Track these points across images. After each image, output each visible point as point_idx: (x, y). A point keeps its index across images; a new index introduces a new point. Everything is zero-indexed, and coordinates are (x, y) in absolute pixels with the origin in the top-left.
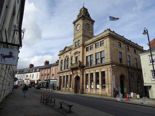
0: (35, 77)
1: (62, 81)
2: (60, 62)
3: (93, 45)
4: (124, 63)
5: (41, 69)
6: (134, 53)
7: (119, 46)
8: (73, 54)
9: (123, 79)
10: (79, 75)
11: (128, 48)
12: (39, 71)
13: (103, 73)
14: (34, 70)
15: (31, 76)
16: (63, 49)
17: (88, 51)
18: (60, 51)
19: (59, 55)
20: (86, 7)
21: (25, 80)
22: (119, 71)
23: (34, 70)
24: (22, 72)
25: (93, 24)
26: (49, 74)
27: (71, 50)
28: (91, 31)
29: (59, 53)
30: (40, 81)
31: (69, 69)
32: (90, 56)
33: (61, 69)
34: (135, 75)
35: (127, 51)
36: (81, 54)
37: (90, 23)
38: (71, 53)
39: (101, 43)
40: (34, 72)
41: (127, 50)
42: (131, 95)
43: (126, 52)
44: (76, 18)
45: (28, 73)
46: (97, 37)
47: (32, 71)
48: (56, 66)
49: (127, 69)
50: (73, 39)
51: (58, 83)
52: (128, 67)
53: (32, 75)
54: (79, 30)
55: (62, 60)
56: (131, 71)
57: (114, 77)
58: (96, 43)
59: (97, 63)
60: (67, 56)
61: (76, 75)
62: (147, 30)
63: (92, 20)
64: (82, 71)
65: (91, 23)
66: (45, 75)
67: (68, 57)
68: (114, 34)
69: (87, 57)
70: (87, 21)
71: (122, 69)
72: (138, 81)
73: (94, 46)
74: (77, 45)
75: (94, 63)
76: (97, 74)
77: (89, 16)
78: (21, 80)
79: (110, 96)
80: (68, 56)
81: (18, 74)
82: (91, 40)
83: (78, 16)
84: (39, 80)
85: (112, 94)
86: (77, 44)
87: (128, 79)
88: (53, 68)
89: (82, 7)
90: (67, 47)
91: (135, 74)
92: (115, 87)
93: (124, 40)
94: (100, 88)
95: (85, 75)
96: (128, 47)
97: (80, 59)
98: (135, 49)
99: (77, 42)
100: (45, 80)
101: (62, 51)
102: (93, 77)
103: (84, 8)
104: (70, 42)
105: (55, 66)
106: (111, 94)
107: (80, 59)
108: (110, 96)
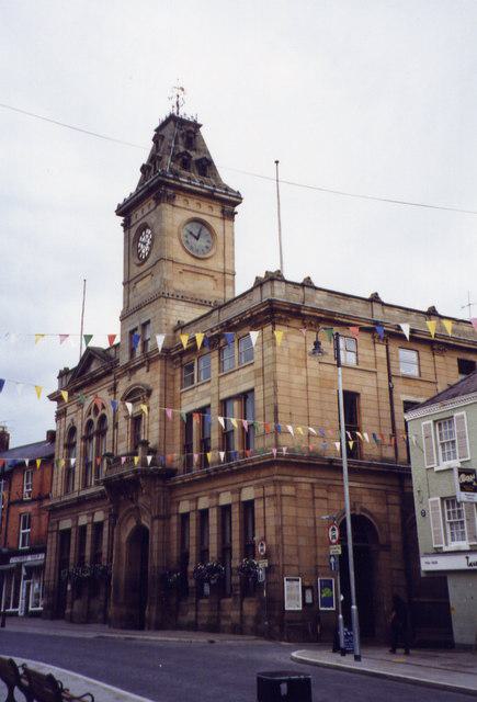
13: (248, 506)
20: (187, 112)
25: (229, 215)
50: (119, 307)
54: (146, 258)
55: (72, 431)
61: (132, 524)
65: (219, 214)
70: (193, 204)
77: (206, 166)
80: (104, 407)
107: (152, 434)
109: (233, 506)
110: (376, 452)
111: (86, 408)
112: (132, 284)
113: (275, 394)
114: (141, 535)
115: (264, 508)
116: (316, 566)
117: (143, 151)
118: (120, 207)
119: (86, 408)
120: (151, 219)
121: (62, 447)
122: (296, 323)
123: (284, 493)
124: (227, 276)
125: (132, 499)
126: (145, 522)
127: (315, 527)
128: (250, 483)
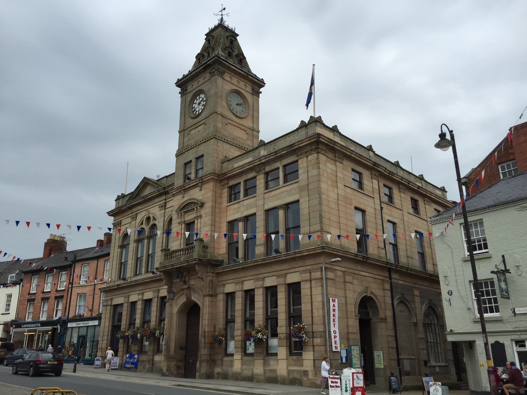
1: (124, 313)
3: (255, 177)
4: (373, 249)
6: (411, 211)
7: (355, 185)
8: (177, 211)
9: (371, 316)
16: (131, 188)
17: (235, 200)
20: (229, 23)
22: (356, 282)
26: (62, 297)
27: (166, 193)
28: (248, 123)
29: (112, 206)
31: (153, 273)
32: (246, 219)
34: (417, 299)
35: (383, 205)
37: (246, 88)
38: (164, 207)
39: (289, 169)
41: (385, 199)
42: (110, 350)
43: (382, 208)
46: (271, 149)
48: (97, 258)
49: (387, 275)
50: (175, 147)
51: (106, 333)
52: (390, 269)
54: (200, 114)
56: (400, 282)
57: (336, 308)
58: (268, 169)
59: (271, 247)
60: (148, 219)
61: (182, 300)
62: (451, 132)
63: (255, 77)
65: (250, 91)
66: (45, 299)
67: (151, 223)
68: (337, 139)
69: (232, 224)
70: (235, 80)
71: (365, 273)
72: (427, 322)
73: (260, 181)
74: (193, 176)
76: (271, 292)
77: (241, 59)
80: (155, 219)
82: (250, 159)
84: (17, 323)
86: (193, 171)
87: (389, 313)
88: (84, 273)
90: (148, 179)
91: (417, 293)
92: (338, 345)
93: (375, 164)
94: (282, 352)
96: (390, 189)
98: (416, 197)
100: (43, 324)
102: (275, 305)
103: (221, 26)
107: (203, 228)
109: (301, 283)
110: (376, 252)
111: (139, 220)
112: (186, 132)
113: (320, 203)
114: (192, 311)
115: (311, 288)
116: (348, 333)
117: (199, 43)
118: (179, 80)
119: (139, 220)
120: (204, 87)
121: (117, 247)
123: (328, 277)
124: (255, 131)
125: (185, 282)
126: (195, 298)
127: (346, 304)
128: (297, 269)
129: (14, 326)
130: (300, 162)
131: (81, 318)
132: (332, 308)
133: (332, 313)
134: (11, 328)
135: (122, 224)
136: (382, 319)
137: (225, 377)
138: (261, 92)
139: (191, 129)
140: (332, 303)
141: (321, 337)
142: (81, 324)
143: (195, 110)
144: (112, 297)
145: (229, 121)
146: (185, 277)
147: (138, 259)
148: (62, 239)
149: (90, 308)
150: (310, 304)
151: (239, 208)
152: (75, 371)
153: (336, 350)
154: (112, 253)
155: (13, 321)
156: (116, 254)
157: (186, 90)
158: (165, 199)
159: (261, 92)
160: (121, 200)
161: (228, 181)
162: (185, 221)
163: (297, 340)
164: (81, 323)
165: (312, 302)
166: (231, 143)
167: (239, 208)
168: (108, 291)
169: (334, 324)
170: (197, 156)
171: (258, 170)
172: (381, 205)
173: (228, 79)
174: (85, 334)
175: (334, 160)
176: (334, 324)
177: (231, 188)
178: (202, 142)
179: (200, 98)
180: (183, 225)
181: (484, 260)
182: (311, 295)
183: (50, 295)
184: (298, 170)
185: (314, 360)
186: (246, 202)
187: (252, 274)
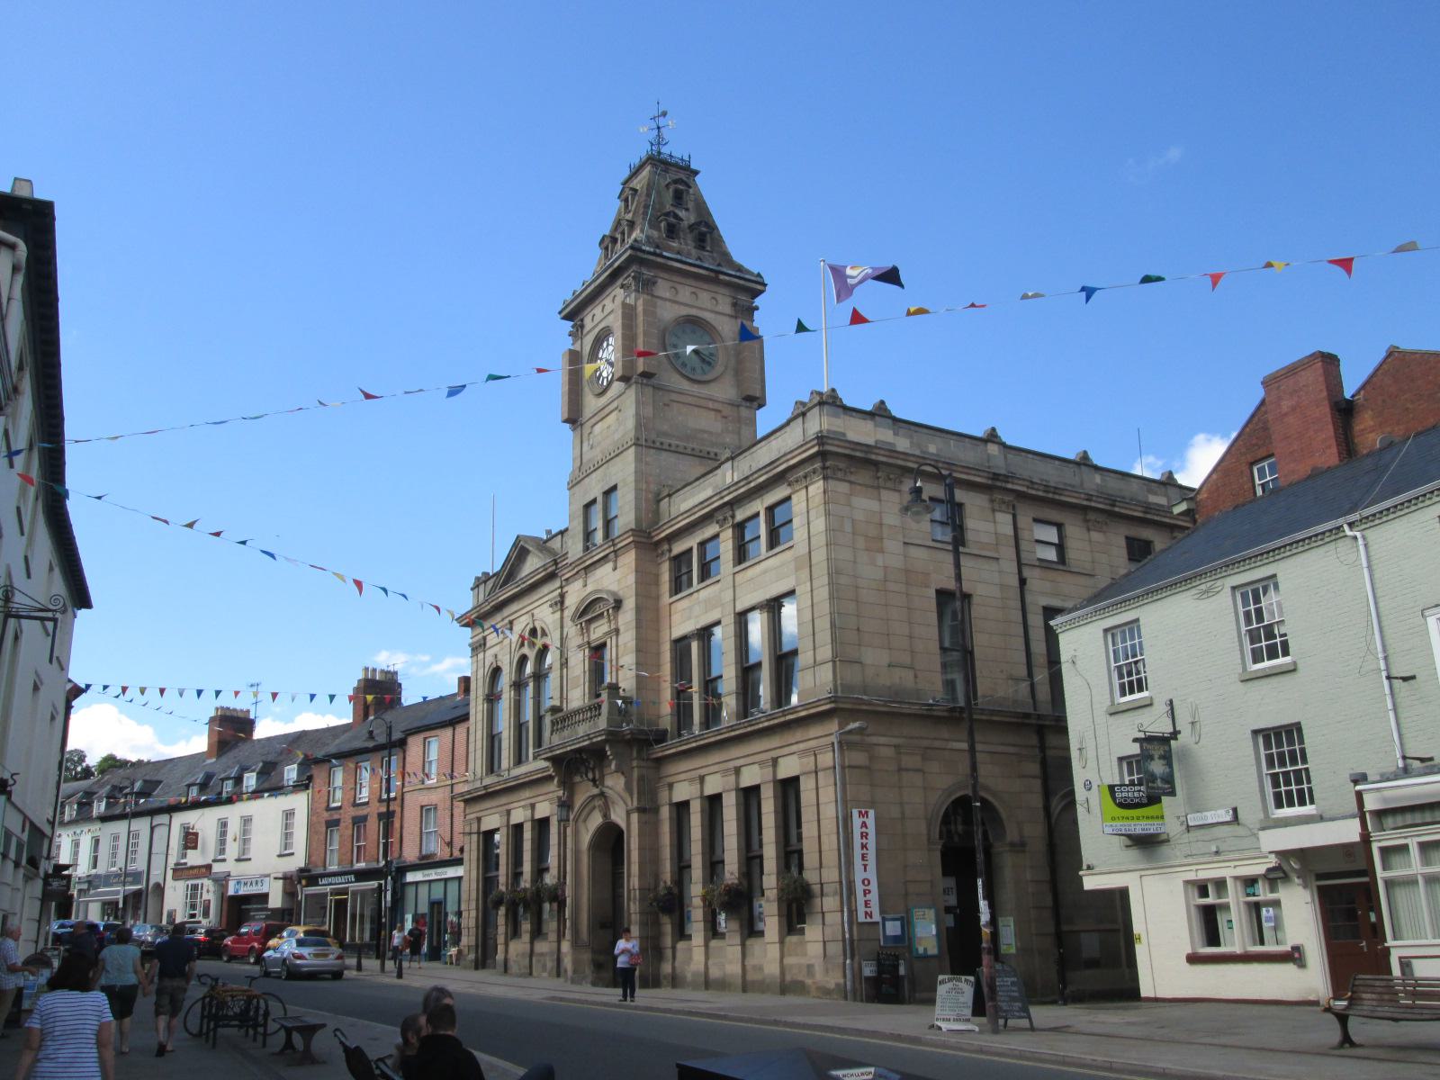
0: (264, 841)
2: (478, 691)
3: (788, 498)
5: (315, 756)
10: (618, 817)
11: (1061, 536)
12: (303, 785)
13: (788, 789)
14: (250, 780)
15: (229, 837)
16: (495, 563)
18: (476, 587)
19: (474, 620)
20: (675, 149)
21: (170, 882)
23: (250, 780)
24: (132, 791)
29: (466, 602)
30: (313, 880)
33: (492, 765)
36: (627, 617)
37: (714, 306)
40: (257, 794)
43: (1023, 582)
44: (586, 264)
45: (196, 805)
47: (238, 780)
49: (1034, 740)
50: (567, 467)
53: (234, 828)
55: (496, 672)
57: (871, 830)
60: (533, 632)
61: (596, 820)
64: (641, 779)
65: (728, 309)
69: (681, 644)
70: (685, 293)
73: (726, 546)
75: (730, 704)
76: (750, 796)
77: (705, 233)
78: (136, 876)
79: (832, 986)
80: (544, 634)
81: (104, 819)
82: (709, 492)
83: (608, 243)
84: (307, 876)
85: (845, 976)
89: (644, 155)
95: (665, 812)
96: (1059, 526)
97: (624, 670)
99: (599, 507)
100: (362, 875)
101: (490, 584)
104: (548, 511)
105: (448, 732)
106: (840, 974)
107: (624, 670)
108: (832, 986)
115: (817, 789)
122: (864, 476)
128: (794, 748)
129: (304, 882)
130: (794, 498)
131: (427, 863)
132: (857, 831)
133: (857, 841)
134: (299, 887)
135: (488, 645)
136: (1012, 845)
137: (675, 981)
138: (757, 308)
139: (593, 421)
140: (857, 821)
141: (835, 894)
142: (433, 874)
143: (601, 374)
144: (532, 801)
145: (674, 396)
146: (593, 770)
147: (519, 727)
148: (389, 676)
149: (448, 839)
150: (816, 823)
151: (690, 608)
152: (400, 976)
153: (869, 920)
154: (472, 712)
155: (301, 870)
156: (479, 716)
157: (582, 327)
158: (561, 587)
159: (757, 308)
160: (482, 587)
161: (670, 545)
162: (589, 643)
163: (121, 905)
164: (432, 871)
165: (819, 821)
166: (681, 450)
167: (690, 608)
168: (471, 800)
169: (865, 866)
170: (606, 488)
171: (721, 518)
172: (1020, 572)
173: (667, 295)
174: (442, 896)
175: (872, 487)
176: (865, 866)
177: (740, 528)
178: (613, 455)
179: (608, 345)
180: (587, 651)
181: (1141, 711)
182: (818, 805)
183: (369, 810)
184: (791, 521)
185: (824, 942)
186: (703, 594)
187: (717, 760)
